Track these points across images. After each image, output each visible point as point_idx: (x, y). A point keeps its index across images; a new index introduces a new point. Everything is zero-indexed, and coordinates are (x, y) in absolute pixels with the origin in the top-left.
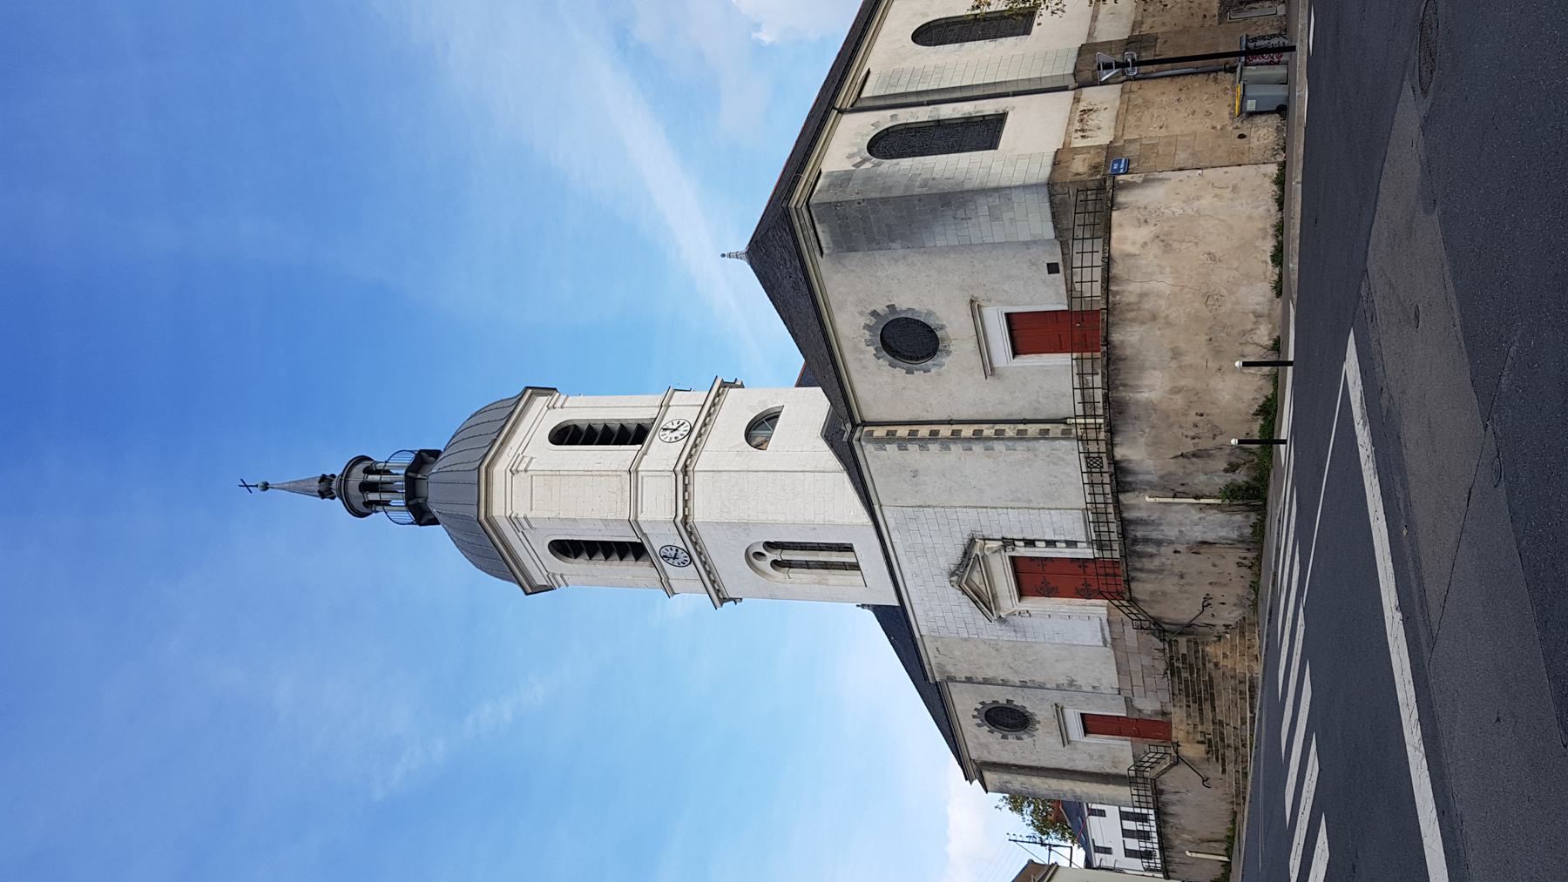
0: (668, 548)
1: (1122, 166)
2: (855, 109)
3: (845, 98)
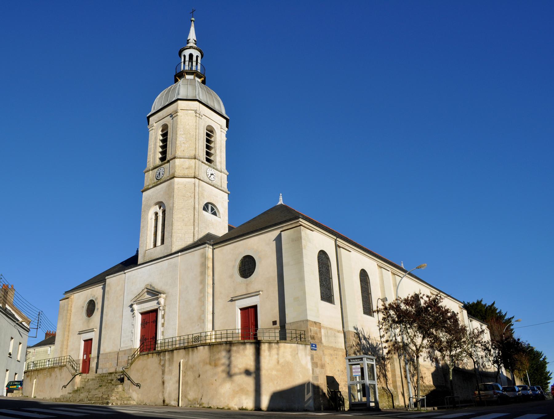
0: (164, 171)
1: (314, 348)
2: (337, 246)
3: (340, 242)
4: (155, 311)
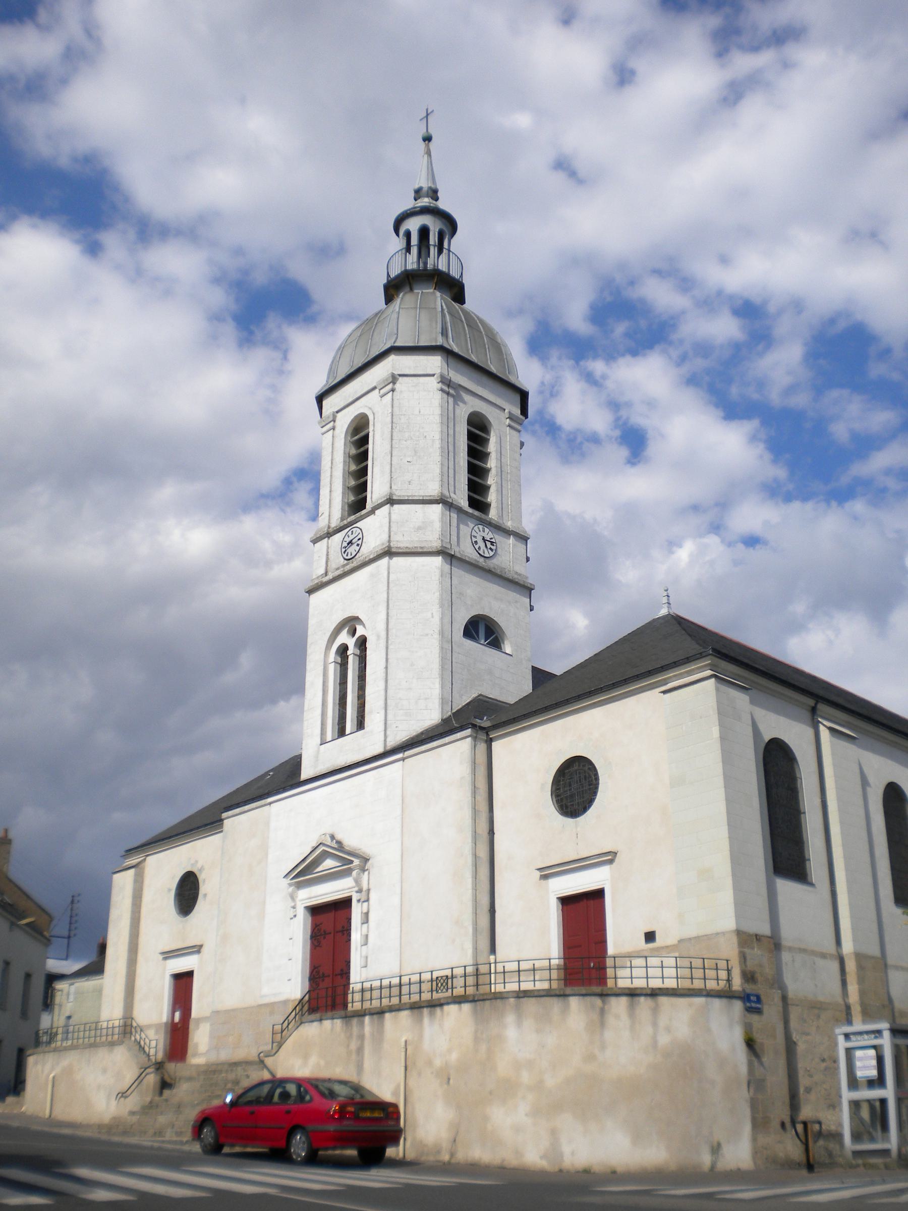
0: (360, 536)
1: (753, 1005)
4: (344, 904)
